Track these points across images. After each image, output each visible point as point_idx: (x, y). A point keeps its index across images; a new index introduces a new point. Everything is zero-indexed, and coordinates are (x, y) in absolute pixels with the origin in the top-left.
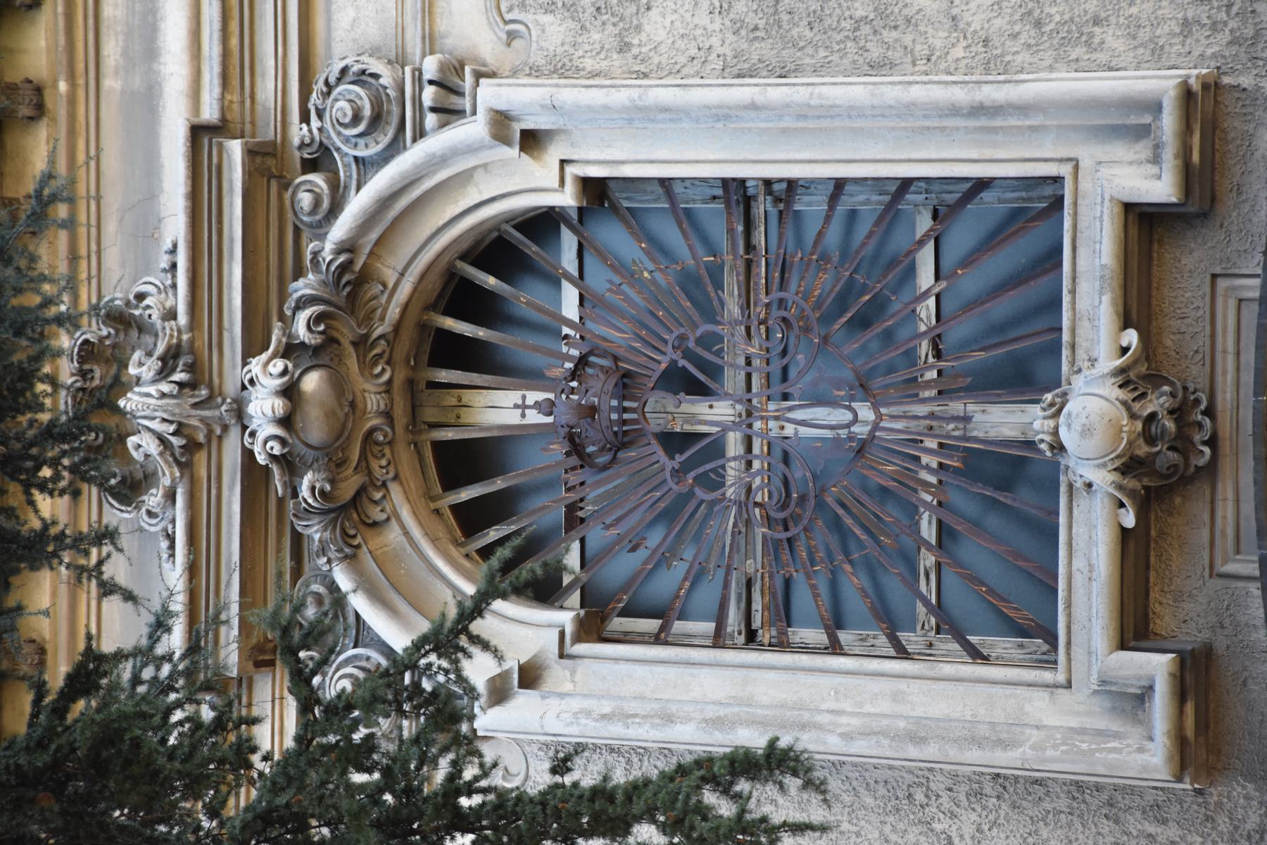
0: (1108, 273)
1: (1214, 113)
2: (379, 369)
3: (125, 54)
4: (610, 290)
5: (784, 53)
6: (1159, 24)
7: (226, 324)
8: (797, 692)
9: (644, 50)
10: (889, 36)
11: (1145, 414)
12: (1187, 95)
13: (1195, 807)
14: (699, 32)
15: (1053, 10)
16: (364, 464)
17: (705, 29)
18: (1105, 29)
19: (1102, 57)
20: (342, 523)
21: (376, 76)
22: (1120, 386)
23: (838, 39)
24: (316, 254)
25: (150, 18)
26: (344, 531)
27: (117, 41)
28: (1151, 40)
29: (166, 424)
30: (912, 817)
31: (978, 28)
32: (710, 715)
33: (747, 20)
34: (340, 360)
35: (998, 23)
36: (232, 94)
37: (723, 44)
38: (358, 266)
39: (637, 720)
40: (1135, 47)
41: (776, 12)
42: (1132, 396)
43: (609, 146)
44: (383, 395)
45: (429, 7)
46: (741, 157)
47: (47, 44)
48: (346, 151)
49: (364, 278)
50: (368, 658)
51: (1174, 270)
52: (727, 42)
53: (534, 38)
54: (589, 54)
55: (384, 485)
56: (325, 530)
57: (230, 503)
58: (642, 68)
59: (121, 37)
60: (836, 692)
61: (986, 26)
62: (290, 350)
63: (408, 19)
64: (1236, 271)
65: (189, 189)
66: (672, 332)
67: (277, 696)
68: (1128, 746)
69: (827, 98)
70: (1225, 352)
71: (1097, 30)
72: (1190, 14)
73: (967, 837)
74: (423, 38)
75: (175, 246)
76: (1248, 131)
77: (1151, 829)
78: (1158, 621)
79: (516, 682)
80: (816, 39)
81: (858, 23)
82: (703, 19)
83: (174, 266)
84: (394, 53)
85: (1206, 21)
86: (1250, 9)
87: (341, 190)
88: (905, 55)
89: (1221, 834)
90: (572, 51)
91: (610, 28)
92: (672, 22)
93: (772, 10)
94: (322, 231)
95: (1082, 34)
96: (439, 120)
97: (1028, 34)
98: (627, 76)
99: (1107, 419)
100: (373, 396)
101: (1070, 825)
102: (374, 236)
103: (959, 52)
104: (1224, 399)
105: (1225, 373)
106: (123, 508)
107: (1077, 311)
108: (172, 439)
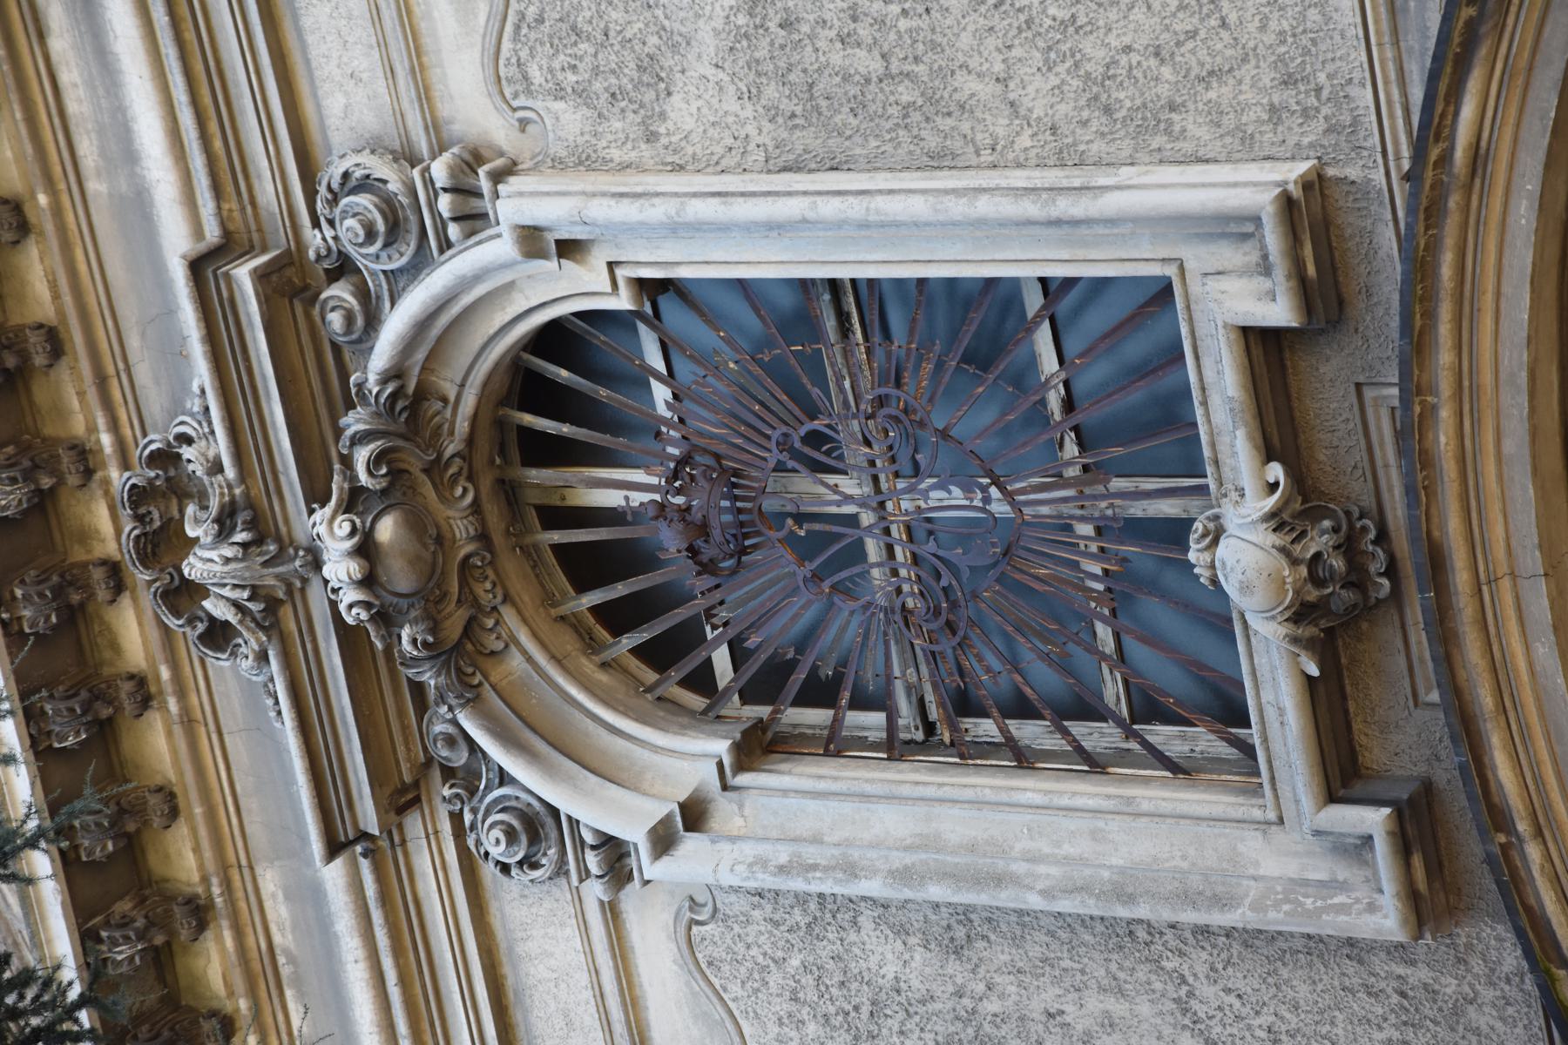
0: (1236, 405)
1: (1323, 207)
2: (459, 491)
3: (103, 152)
4: (696, 382)
5: (831, 142)
6: (1243, 110)
7: (280, 467)
8: (986, 829)
9: (674, 139)
10: (945, 123)
11: (1309, 556)
12: (1287, 204)
13: (1443, 948)
14: (731, 119)
15: (1122, 95)
16: (466, 590)
17: (736, 116)
18: (1184, 115)
19: (1187, 147)
20: (457, 663)
21: (385, 182)
22: (1274, 530)
23: (888, 127)
24: (360, 386)
25: (120, 116)
26: (459, 670)
27: (90, 139)
28: (1237, 128)
29: (238, 590)
30: (1137, 955)
31: (1042, 114)
32: (897, 865)
33: (781, 107)
34: (415, 490)
35: (1063, 108)
36: (229, 201)
37: (762, 134)
38: (411, 387)
39: (818, 874)
40: (1221, 136)
41: (812, 98)
42: (1289, 538)
43: (658, 248)
44: (471, 518)
45: (426, 93)
46: (806, 259)
47: (14, 153)
48: (373, 262)
49: (423, 393)
50: (517, 798)
51: (1313, 379)
52: (765, 130)
53: (549, 127)
54: (613, 145)
55: (494, 609)
56: (438, 674)
57: (329, 656)
58: (676, 159)
59: (93, 136)
60: (1029, 830)
61: (1050, 112)
62: (355, 500)
63: (406, 105)
64: (1383, 380)
65: (204, 332)
66: (774, 428)
67: (430, 831)
68: (1357, 901)
69: (886, 214)
70: (1386, 466)
71: (1175, 117)
72: (1276, 99)
73: (1201, 975)
74: (426, 128)
75: (203, 391)
76: (1365, 228)
77: (1400, 970)
78: (1367, 754)
79: (680, 825)
80: (863, 127)
81: (907, 109)
82: (732, 105)
83: (207, 409)
84: (397, 143)
85: (1295, 107)
86: (1342, 94)
87: (374, 301)
88: (967, 144)
89: (1477, 976)
90: (594, 141)
91: (631, 116)
92: (699, 109)
93: (807, 96)
94: (364, 346)
95: (1159, 122)
96: (462, 231)
97: (1098, 122)
98: (661, 167)
99: (1265, 574)
100: (459, 522)
101: (1310, 965)
102: (420, 356)
103: (1025, 141)
104: (1396, 517)
105: (1390, 489)
106: (219, 656)
107: (1214, 425)
108: (249, 605)
